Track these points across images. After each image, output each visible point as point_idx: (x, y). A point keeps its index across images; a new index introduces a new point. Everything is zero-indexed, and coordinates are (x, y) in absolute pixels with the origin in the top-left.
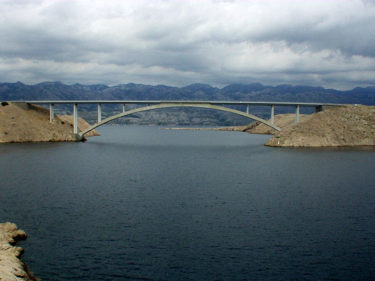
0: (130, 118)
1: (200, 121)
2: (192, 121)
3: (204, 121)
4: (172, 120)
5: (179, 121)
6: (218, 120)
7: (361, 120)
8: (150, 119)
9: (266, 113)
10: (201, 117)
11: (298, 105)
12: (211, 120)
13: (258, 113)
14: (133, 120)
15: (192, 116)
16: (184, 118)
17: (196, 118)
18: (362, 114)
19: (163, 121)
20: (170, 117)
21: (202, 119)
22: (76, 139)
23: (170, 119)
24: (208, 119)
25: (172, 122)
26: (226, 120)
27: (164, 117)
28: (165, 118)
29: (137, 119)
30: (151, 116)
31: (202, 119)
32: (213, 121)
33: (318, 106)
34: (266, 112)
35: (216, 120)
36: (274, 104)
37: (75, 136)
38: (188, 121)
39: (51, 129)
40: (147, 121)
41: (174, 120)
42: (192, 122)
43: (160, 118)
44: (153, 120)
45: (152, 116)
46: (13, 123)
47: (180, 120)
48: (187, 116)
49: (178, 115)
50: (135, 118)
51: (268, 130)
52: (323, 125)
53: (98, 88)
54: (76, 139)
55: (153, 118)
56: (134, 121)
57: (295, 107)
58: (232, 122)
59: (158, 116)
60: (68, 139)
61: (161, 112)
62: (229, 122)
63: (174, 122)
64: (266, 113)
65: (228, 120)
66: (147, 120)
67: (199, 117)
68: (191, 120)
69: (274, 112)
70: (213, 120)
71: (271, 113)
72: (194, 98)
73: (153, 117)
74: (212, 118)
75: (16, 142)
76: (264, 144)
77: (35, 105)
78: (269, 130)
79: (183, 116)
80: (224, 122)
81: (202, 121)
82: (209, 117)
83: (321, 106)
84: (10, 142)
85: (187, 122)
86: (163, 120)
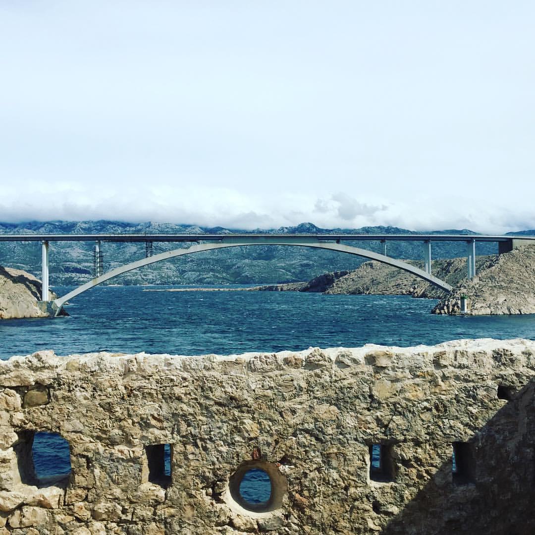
0: (74, 275)
4: (150, 277)
5: (162, 277)
14: (79, 278)
16: (170, 273)
21: (201, 273)
22: (48, 314)
23: (145, 275)
24: (211, 273)
25: (150, 279)
29: (87, 275)
36: (475, 237)
38: (177, 277)
41: (153, 276)
47: (163, 275)
48: (174, 268)
49: (160, 268)
50: (83, 275)
54: (48, 314)
56: (82, 279)
57: (465, 243)
63: (153, 279)
67: (194, 271)
71: (42, 271)
72: (390, 232)
74: (219, 272)
76: (417, 353)
79: (167, 269)
80: (239, 278)
81: (201, 277)
82: (212, 270)
85: (175, 279)
86: (134, 276)
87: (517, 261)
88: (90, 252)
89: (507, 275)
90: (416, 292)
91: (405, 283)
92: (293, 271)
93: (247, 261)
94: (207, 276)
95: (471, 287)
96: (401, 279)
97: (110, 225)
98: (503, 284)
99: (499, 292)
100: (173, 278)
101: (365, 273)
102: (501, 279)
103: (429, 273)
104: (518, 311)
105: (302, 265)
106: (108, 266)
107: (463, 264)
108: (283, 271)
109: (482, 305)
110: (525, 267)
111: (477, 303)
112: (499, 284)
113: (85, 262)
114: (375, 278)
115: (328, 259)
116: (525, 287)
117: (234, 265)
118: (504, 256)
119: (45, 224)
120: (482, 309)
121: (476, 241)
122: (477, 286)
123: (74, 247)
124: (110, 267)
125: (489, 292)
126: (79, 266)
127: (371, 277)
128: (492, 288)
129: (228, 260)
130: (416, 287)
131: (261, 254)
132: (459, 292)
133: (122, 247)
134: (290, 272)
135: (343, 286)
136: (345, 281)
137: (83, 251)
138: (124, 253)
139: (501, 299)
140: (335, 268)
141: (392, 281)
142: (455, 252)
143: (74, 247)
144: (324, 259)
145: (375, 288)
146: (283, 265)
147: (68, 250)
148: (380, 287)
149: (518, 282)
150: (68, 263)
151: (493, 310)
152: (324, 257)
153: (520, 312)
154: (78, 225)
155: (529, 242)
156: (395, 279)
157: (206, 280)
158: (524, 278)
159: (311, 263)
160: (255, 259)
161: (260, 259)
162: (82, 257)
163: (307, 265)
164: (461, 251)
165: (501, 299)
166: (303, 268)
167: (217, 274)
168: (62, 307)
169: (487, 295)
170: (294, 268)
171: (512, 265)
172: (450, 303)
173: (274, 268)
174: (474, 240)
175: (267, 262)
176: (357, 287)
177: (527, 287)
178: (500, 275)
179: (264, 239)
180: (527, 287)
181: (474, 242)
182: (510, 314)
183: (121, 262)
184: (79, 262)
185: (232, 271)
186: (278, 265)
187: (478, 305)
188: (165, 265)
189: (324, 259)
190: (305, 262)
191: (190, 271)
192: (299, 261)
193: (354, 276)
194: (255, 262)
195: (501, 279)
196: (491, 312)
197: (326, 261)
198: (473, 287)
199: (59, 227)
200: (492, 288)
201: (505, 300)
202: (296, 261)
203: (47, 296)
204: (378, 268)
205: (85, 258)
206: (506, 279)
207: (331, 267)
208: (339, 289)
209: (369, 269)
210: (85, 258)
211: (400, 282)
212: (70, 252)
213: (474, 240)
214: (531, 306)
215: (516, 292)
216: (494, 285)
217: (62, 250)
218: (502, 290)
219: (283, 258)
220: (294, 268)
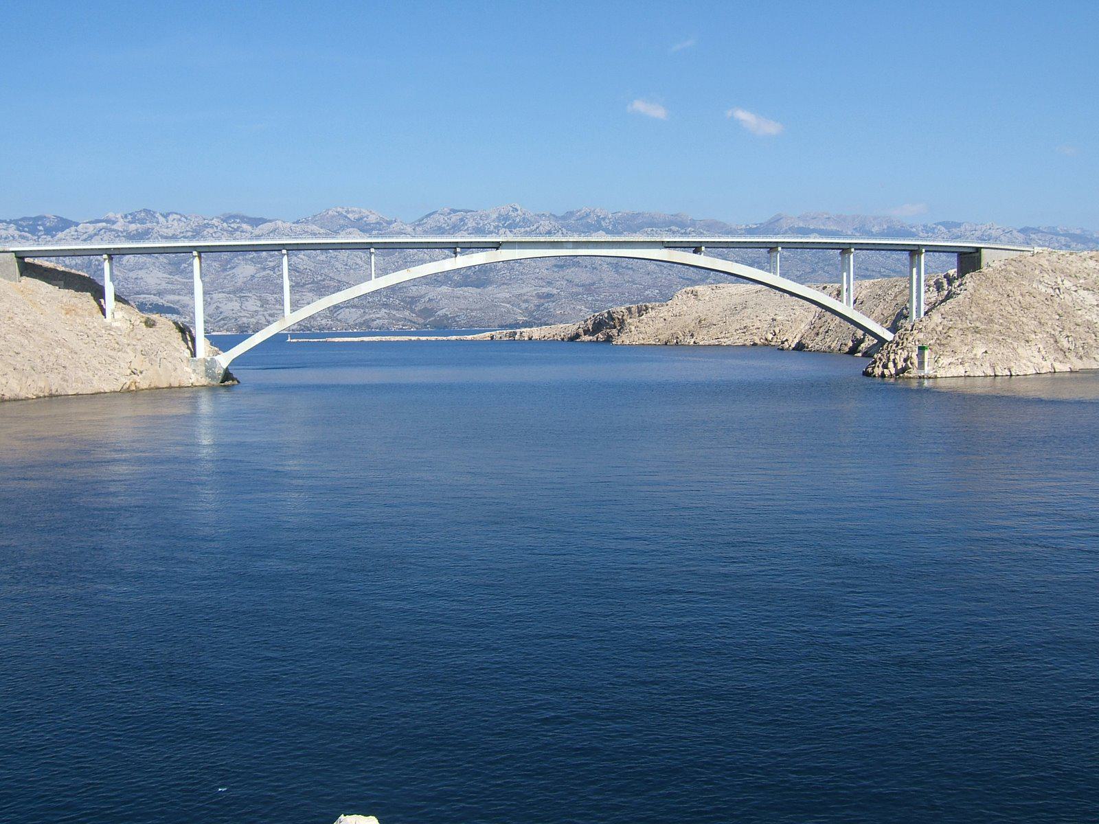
1: (361, 317)
2: (339, 317)
6: (413, 311)
7: (1081, 292)
12: (394, 312)
18: (1078, 275)
19: (253, 320)
20: (270, 309)
27: (255, 308)
28: (256, 311)
30: (215, 305)
35: (407, 313)
39: (116, 346)
43: (243, 314)
44: (223, 319)
45: (218, 308)
53: (41, 228)
58: (454, 317)
59: (235, 305)
60: (180, 384)
69: (292, 305)
73: (221, 310)
75: (10, 400)
80: (432, 319)
81: (367, 317)
82: (385, 305)
83: (978, 250)
85: (323, 322)
87: (993, 286)
88: (176, 277)
89: (982, 311)
90: (787, 340)
91: (758, 324)
92: (524, 305)
93: (444, 289)
94: (378, 316)
95: (929, 330)
96: (748, 317)
97: (207, 230)
98: (978, 324)
99: (974, 338)
100: (319, 319)
101: (685, 308)
102: (974, 316)
103: (848, 303)
104: (1006, 370)
105: (539, 296)
106: (209, 300)
107: (864, 292)
108: (508, 305)
109: (950, 360)
110: (1006, 296)
111: (942, 357)
112: (973, 325)
113: (170, 294)
114: (703, 317)
115: (583, 286)
116: (1011, 329)
117: (422, 297)
118: (972, 277)
119: (101, 230)
120: (952, 366)
121: (926, 251)
122: (940, 328)
123: (151, 269)
124: (213, 301)
125: (959, 339)
126: (161, 301)
127: (697, 315)
128: (964, 331)
129: (412, 288)
130: (777, 332)
131: (468, 276)
132: (911, 339)
133: (229, 266)
134: (519, 307)
135: (648, 330)
136: (651, 323)
137: (165, 275)
138: (232, 277)
139: (979, 351)
140: (597, 300)
141: (733, 321)
142: (798, 273)
143: (151, 269)
144: (577, 285)
145: (705, 332)
146: (507, 295)
147: (141, 273)
148: (713, 330)
149: (1001, 321)
150: (142, 296)
151: (968, 369)
152: (577, 281)
153: (1010, 371)
154: (155, 231)
155: (1005, 254)
156: (738, 317)
157: (375, 323)
158: (1009, 316)
159: (555, 291)
160: (458, 285)
161: (466, 286)
162: (164, 285)
163: (549, 296)
164: (808, 270)
165: (979, 351)
166: (542, 301)
167: (394, 312)
168: (227, 368)
169: (956, 343)
170: (526, 301)
171: (987, 293)
172: (897, 357)
173: (492, 301)
174: (924, 251)
175: (479, 290)
176: (673, 331)
177: (1014, 330)
178: (973, 309)
179: (571, 245)
180: (1014, 330)
181: (922, 253)
182: (996, 376)
183: (229, 293)
184: (160, 294)
185: (419, 307)
186: (498, 295)
187: (944, 361)
188: (304, 297)
189: (577, 285)
190: (545, 290)
191: (347, 307)
192: (534, 288)
193: (666, 313)
194: (459, 291)
195: (974, 316)
196: (966, 372)
197: (581, 289)
198: (934, 329)
199: (125, 234)
200: (964, 331)
201: (986, 352)
202: (529, 289)
203: (202, 345)
204: (707, 298)
205: (170, 286)
206: (982, 316)
207: (590, 299)
208: (641, 336)
209: (692, 301)
210: (170, 286)
211: (747, 322)
212: (143, 277)
213: (924, 251)
214: (1024, 361)
215: (1000, 338)
216: (965, 326)
217: (131, 274)
218: (978, 335)
219: (506, 284)
220: (526, 301)
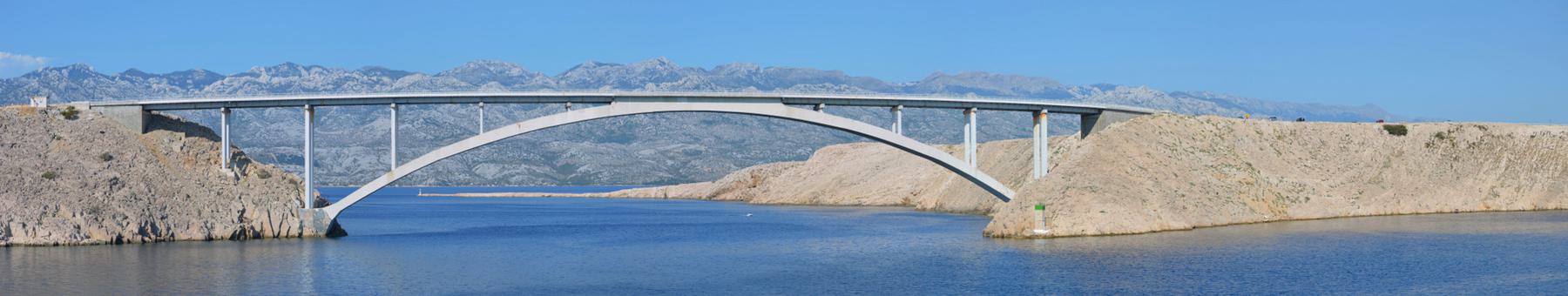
3: (514, 171)
6: (553, 167)
8: (348, 168)
9: (692, 147)
10: (503, 162)
11: (1043, 107)
12: (534, 168)
13: (669, 148)
15: (475, 159)
17: (485, 165)
21: (506, 166)
24: (523, 165)
26: (578, 168)
31: (506, 166)
32: (538, 171)
33: (1093, 112)
34: (690, 143)
35: (547, 169)
37: (312, 219)
40: (340, 174)
42: (476, 175)
44: (360, 172)
46: (112, 174)
51: (813, 190)
52: (1129, 170)
55: (359, 166)
58: (596, 174)
61: (380, 148)
62: (587, 173)
63: (422, 176)
64: (692, 147)
65: (582, 169)
66: (342, 172)
67: (493, 161)
68: (473, 170)
70: (538, 170)
73: (359, 163)
74: (535, 163)
77: (162, 113)
78: (813, 193)
81: (506, 172)
82: (526, 161)
84: (1451, 212)
